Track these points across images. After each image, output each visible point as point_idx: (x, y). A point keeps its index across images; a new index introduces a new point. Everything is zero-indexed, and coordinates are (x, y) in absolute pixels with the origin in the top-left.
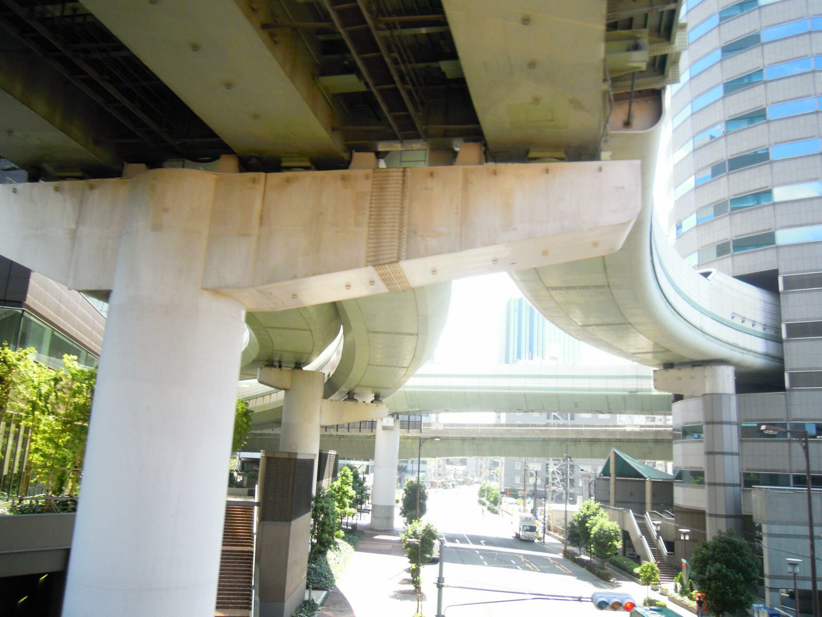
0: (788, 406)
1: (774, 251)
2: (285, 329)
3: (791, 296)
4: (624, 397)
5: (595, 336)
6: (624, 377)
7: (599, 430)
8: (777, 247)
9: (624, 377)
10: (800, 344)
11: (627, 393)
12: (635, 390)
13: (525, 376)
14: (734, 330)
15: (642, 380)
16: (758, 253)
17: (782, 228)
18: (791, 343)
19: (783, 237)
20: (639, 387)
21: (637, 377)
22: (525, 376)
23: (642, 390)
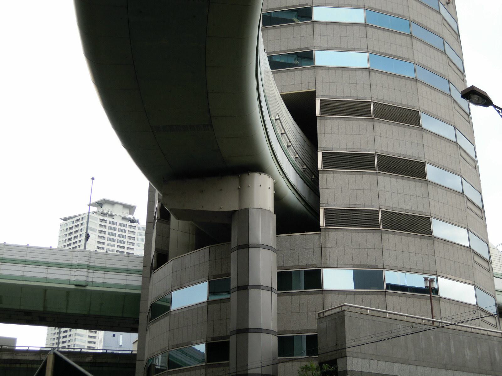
0: (323, 249)
1: (312, 71)
2: (298, 200)
3: (328, 122)
4: (68, 292)
5: (111, 216)
6: (71, 266)
7: (326, 115)
8: (315, 68)
9: (71, 266)
10: (337, 176)
11: (73, 287)
12: (84, 284)
13: (9, 265)
14: (118, 275)
15: (18, 308)
16: (292, 73)
17: (321, 49)
18: (328, 175)
19: (322, 58)
20: (90, 280)
21: (89, 267)
22: (9, 265)
23: (93, 284)
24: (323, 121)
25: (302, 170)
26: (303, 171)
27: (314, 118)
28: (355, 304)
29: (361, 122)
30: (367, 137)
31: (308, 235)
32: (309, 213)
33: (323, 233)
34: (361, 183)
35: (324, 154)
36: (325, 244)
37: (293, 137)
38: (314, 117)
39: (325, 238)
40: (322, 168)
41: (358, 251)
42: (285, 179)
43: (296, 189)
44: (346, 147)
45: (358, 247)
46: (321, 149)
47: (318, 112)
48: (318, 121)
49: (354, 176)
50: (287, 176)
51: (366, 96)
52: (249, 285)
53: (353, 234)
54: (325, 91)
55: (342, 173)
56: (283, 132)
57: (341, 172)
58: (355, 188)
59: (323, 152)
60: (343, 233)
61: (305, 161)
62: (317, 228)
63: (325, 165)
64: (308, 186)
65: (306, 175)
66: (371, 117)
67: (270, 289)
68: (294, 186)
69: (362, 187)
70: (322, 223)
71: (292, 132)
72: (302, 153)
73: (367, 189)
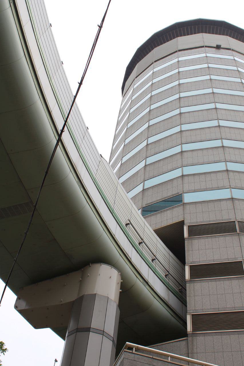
18: (195, 284)
24: (190, 241)
25: (178, 291)
26: (180, 292)
27: (182, 240)
28: (188, 357)
29: (227, 237)
30: (234, 248)
31: (175, 343)
32: (173, 318)
33: (190, 339)
34: (230, 288)
35: (191, 267)
36: (193, 349)
37: (164, 258)
38: (183, 239)
39: (193, 343)
40: (189, 279)
41: (230, 354)
42: (82, 189)
43: (168, 304)
44: (213, 259)
45: (230, 350)
46: (188, 263)
47: (186, 234)
48: (186, 242)
49: (222, 282)
50: (149, 283)
51: (231, 218)
52: (91, 327)
53: (224, 337)
54: (192, 218)
55: (210, 281)
56: (141, 241)
57: (209, 281)
58: (224, 293)
59: (190, 266)
60: (212, 336)
61: (172, 273)
62: (183, 334)
63: (192, 275)
64: (177, 297)
65: (170, 283)
66: (237, 232)
67: (108, 336)
68: (163, 299)
69: (232, 291)
70: (189, 328)
71: (162, 254)
72: (180, 278)
73: (236, 292)
